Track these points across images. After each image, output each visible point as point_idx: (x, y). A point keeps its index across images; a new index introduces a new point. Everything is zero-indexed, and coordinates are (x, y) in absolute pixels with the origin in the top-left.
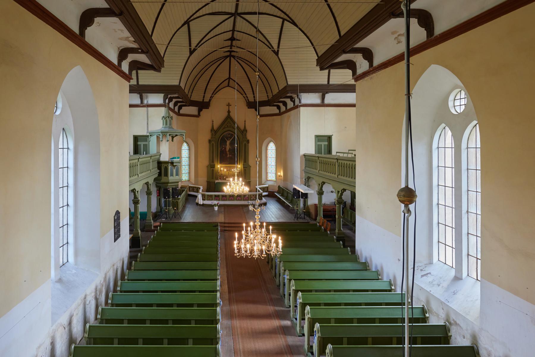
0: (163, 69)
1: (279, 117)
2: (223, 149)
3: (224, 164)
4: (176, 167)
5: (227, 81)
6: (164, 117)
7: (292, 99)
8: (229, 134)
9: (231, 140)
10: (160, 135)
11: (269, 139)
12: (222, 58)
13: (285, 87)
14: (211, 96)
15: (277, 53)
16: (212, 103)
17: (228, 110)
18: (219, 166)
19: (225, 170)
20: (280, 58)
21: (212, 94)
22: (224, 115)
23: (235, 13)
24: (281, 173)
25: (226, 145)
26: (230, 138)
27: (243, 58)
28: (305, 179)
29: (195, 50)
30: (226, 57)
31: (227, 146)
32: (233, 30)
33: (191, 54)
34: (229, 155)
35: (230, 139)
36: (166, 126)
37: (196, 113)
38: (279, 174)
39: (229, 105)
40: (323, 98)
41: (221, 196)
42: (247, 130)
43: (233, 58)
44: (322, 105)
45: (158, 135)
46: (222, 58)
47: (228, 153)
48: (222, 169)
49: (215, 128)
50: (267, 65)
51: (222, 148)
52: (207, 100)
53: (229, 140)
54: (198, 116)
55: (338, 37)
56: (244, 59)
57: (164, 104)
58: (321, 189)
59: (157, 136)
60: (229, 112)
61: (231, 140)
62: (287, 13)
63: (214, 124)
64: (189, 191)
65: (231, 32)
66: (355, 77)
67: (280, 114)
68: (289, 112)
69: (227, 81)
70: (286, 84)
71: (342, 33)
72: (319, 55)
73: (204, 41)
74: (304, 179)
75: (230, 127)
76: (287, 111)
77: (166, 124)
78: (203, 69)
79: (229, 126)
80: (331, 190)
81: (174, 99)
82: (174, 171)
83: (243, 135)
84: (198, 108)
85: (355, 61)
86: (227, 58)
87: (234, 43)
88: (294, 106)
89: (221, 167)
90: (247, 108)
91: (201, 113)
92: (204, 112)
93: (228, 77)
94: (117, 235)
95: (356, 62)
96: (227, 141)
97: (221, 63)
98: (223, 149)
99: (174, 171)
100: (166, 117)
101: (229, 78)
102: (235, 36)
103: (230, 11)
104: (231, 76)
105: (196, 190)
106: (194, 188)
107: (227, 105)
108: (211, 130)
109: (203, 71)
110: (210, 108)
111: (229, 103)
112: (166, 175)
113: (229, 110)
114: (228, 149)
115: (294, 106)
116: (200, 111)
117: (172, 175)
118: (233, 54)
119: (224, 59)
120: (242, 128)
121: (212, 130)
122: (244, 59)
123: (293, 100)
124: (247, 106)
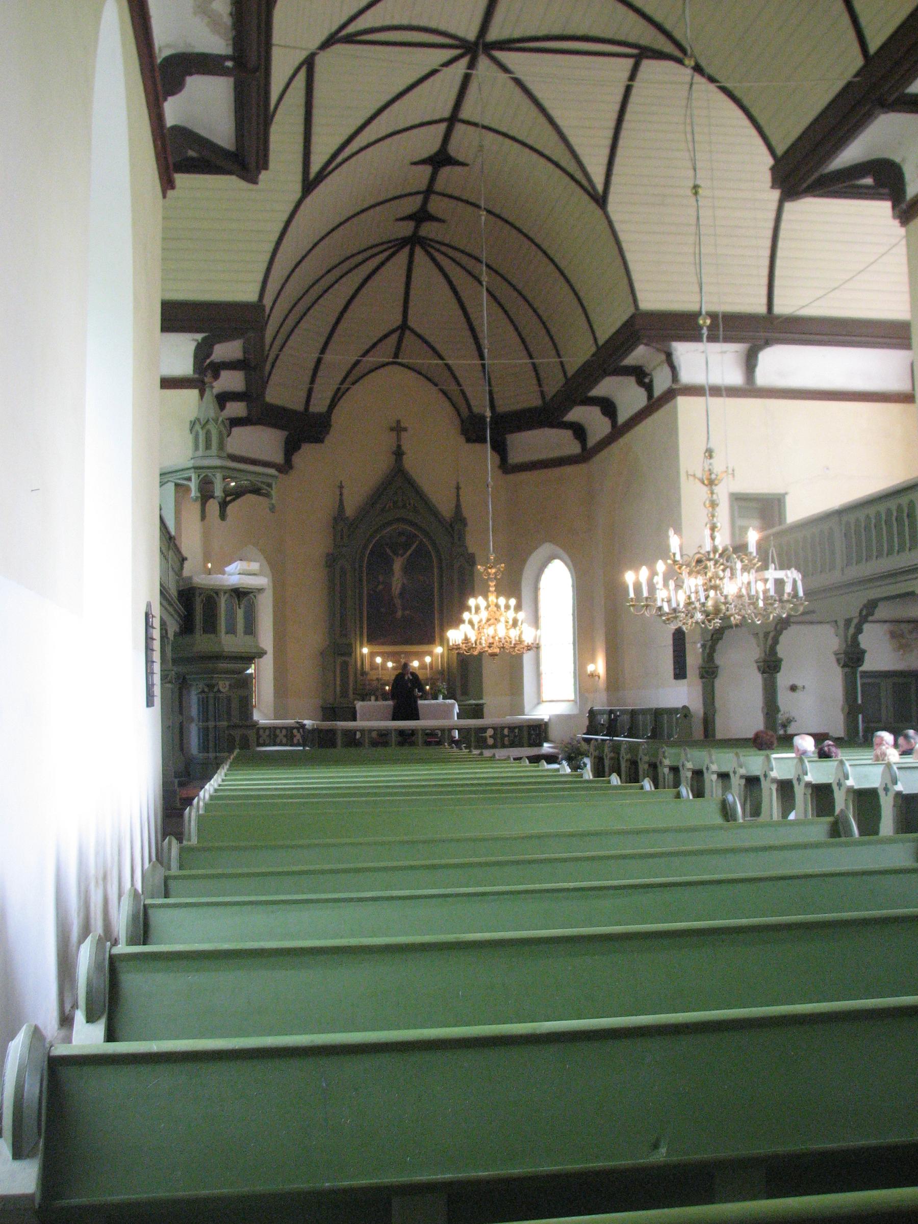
0: (263, 176)
1: (582, 468)
2: (381, 587)
3: (383, 644)
4: (244, 601)
5: (395, 337)
6: (198, 419)
7: (641, 375)
8: (401, 534)
9: (409, 552)
10: (189, 479)
11: (546, 549)
12: (385, 247)
13: (629, 324)
14: (339, 389)
15: (601, 201)
16: (339, 418)
17: (395, 445)
18: (365, 650)
19: (390, 665)
20: (614, 217)
21: (343, 382)
22: (381, 465)
23: (476, 44)
24: (598, 666)
25: (390, 571)
26: (407, 546)
27: (462, 248)
28: (703, 646)
29: (322, 176)
30: (402, 243)
31: (395, 579)
32: (453, 119)
33: (308, 189)
34: (404, 609)
35: (405, 553)
36: (208, 453)
37: (278, 457)
38: (590, 668)
39: (398, 429)
40: (750, 363)
41: (393, 744)
42: (466, 524)
43: (423, 248)
44: (750, 391)
45: (179, 481)
46: (385, 247)
47: (398, 602)
48: (379, 660)
49: (350, 511)
50: (525, 293)
51: (376, 587)
52: (319, 406)
53: (402, 556)
54: (286, 467)
55: (859, 62)
56: (462, 252)
57: (197, 376)
58: (772, 651)
59: (177, 485)
60: (399, 454)
61: (409, 552)
62: (668, 26)
63: (345, 497)
64: (259, 745)
65: (443, 126)
66: (904, 206)
67: (586, 455)
68: (628, 431)
69: (395, 336)
70: (632, 310)
71: (873, 48)
72: (780, 151)
73: (354, 150)
74: (699, 645)
75: (404, 506)
76: (618, 431)
77: (208, 446)
78: (318, 281)
79: (400, 504)
80: (791, 683)
81: (223, 369)
82: (240, 613)
83: (452, 536)
84: (286, 433)
85: (897, 159)
86: (402, 248)
87: (446, 172)
88: (651, 402)
89: (373, 655)
90: (462, 439)
91: (297, 459)
92: (307, 454)
93: (397, 320)
94: (150, 703)
95: (901, 165)
96: (395, 558)
97: (378, 268)
98: (381, 587)
99: (240, 613)
100: (208, 421)
101: (404, 327)
102: (453, 150)
103: (461, 34)
104: (409, 317)
105: (286, 736)
106: (278, 731)
107: (392, 429)
108: (335, 519)
109: (318, 289)
110: (330, 439)
111: (398, 422)
112: (211, 626)
113: (399, 446)
114: (399, 585)
115: (651, 402)
116: (291, 448)
117: (231, 630)
118: (428, 230)
119: (386, 254)
120: (446, 509)
121: (339, 517)
122: (462, 252)
123: (647, 380)
124: (462, 434)
